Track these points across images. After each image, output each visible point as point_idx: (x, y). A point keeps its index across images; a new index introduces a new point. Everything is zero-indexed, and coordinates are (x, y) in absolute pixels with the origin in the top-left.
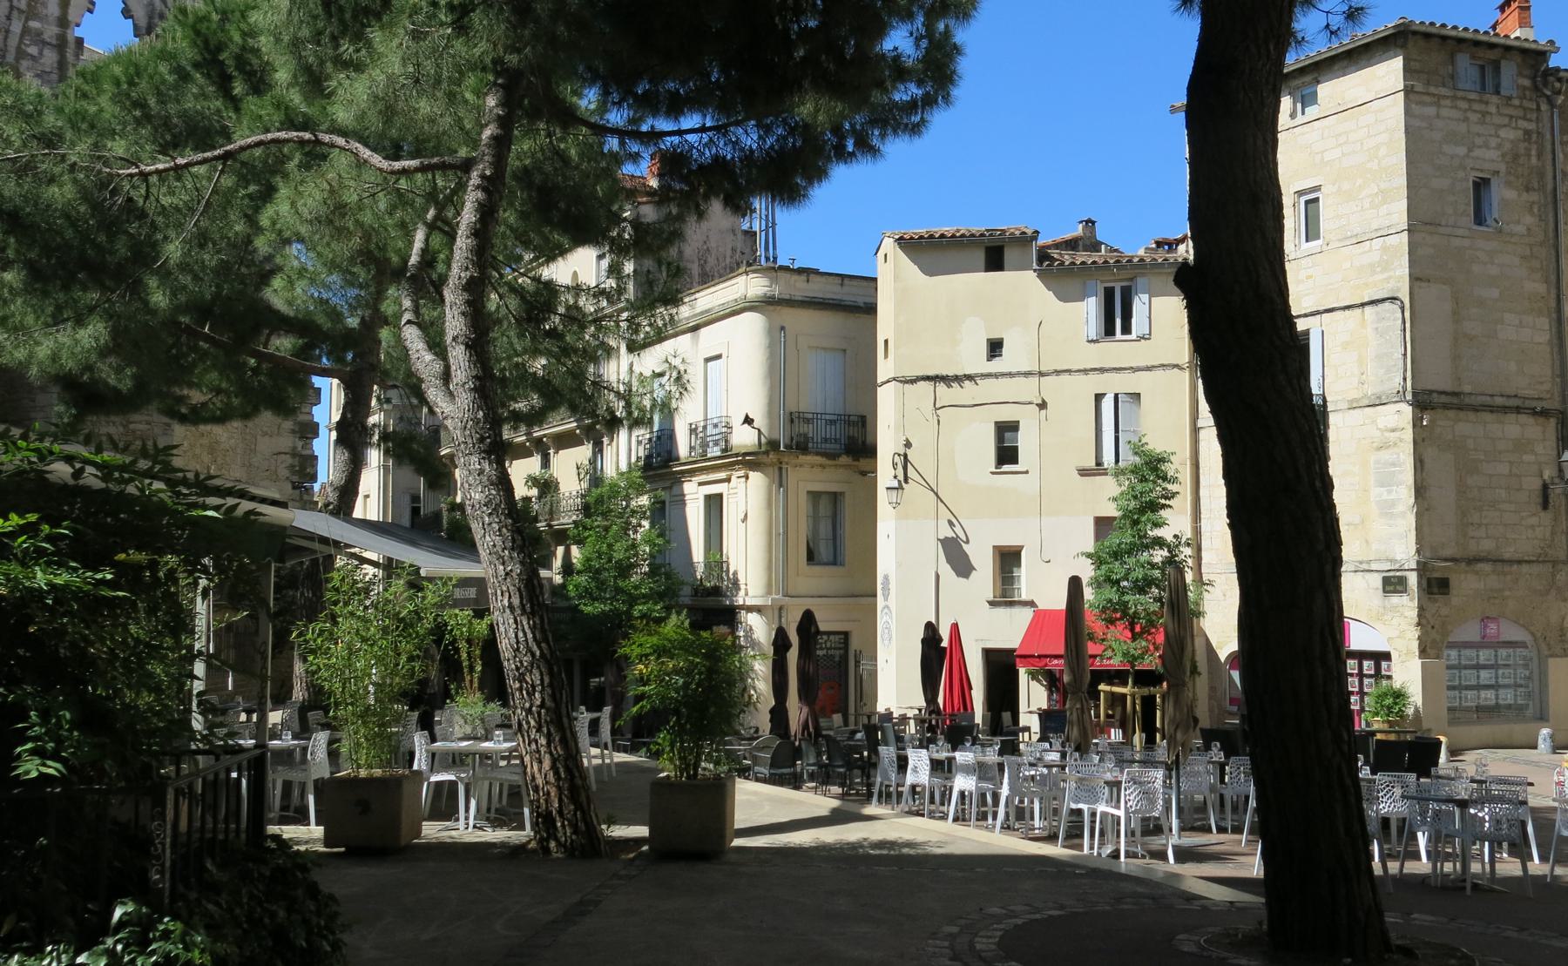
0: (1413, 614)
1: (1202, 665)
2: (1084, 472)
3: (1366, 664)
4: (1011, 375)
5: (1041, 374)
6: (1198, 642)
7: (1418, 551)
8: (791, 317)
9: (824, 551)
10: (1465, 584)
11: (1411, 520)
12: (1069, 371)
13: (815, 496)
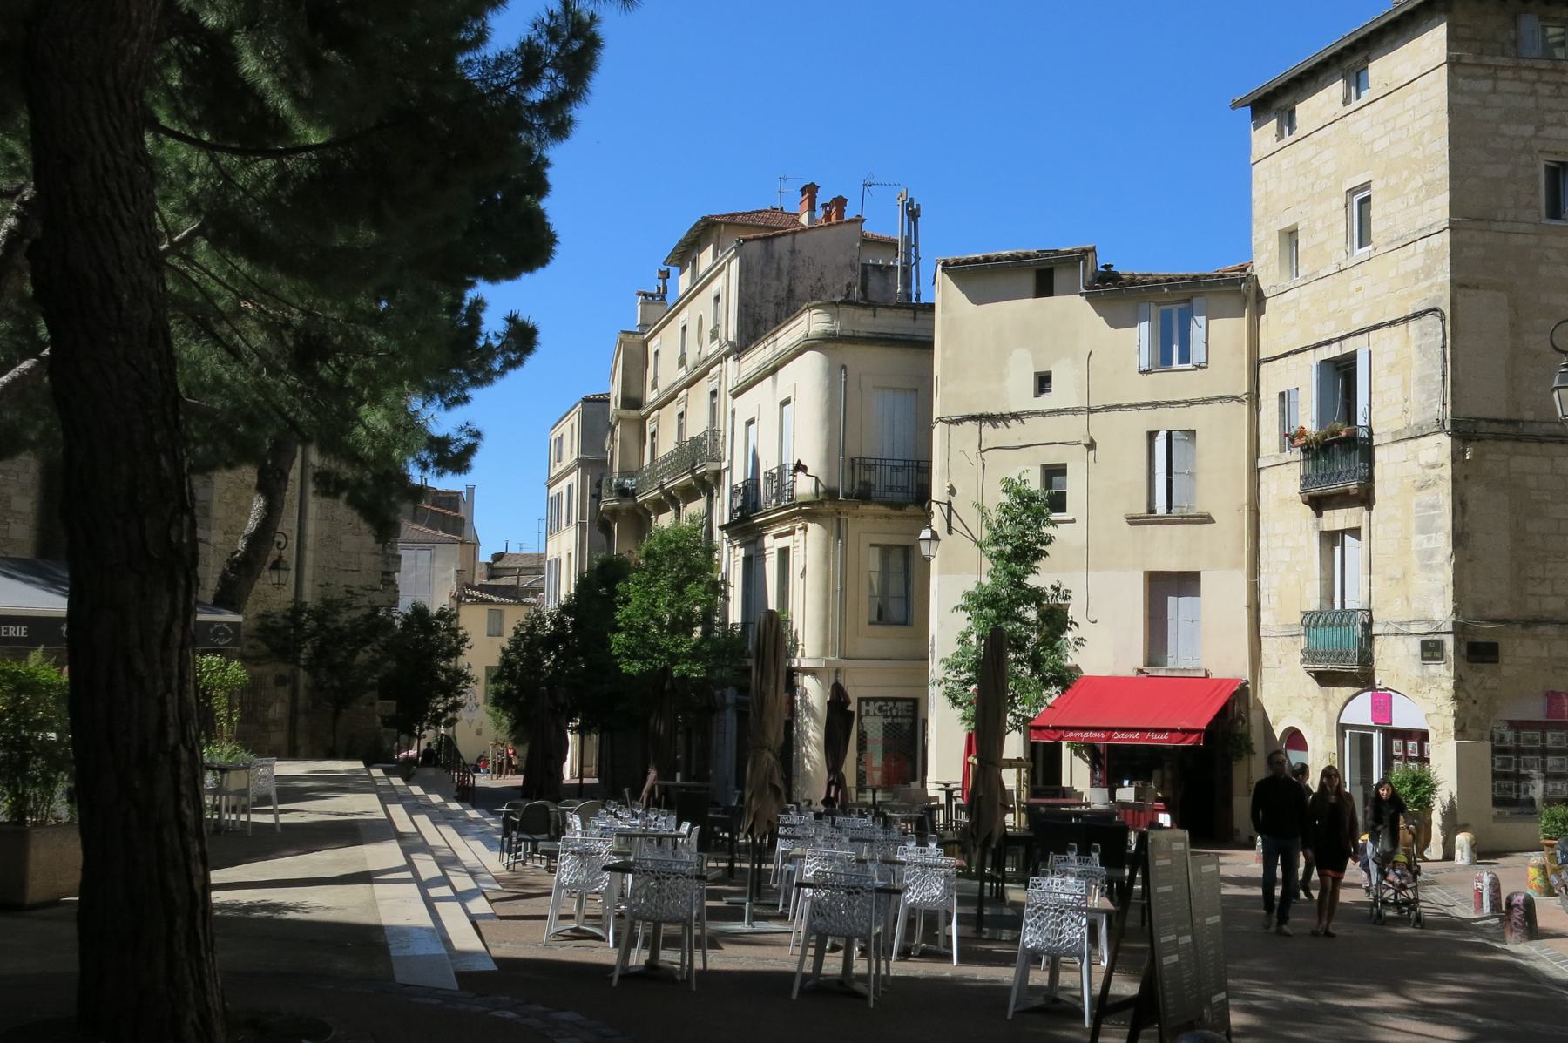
0: (1448, 685)
1: (1256, 738)
2: (1134, 521)
3: (1410, 744)
4: (1058, 412)
5: (1090, 411)
6: (1254, 717)
7: (1456, 611)
8: (852, 354)
9: (895, 609)
10: (1520, 652)
11: (1448, 573)
12: (1119, 407)
13: (886, 550)
